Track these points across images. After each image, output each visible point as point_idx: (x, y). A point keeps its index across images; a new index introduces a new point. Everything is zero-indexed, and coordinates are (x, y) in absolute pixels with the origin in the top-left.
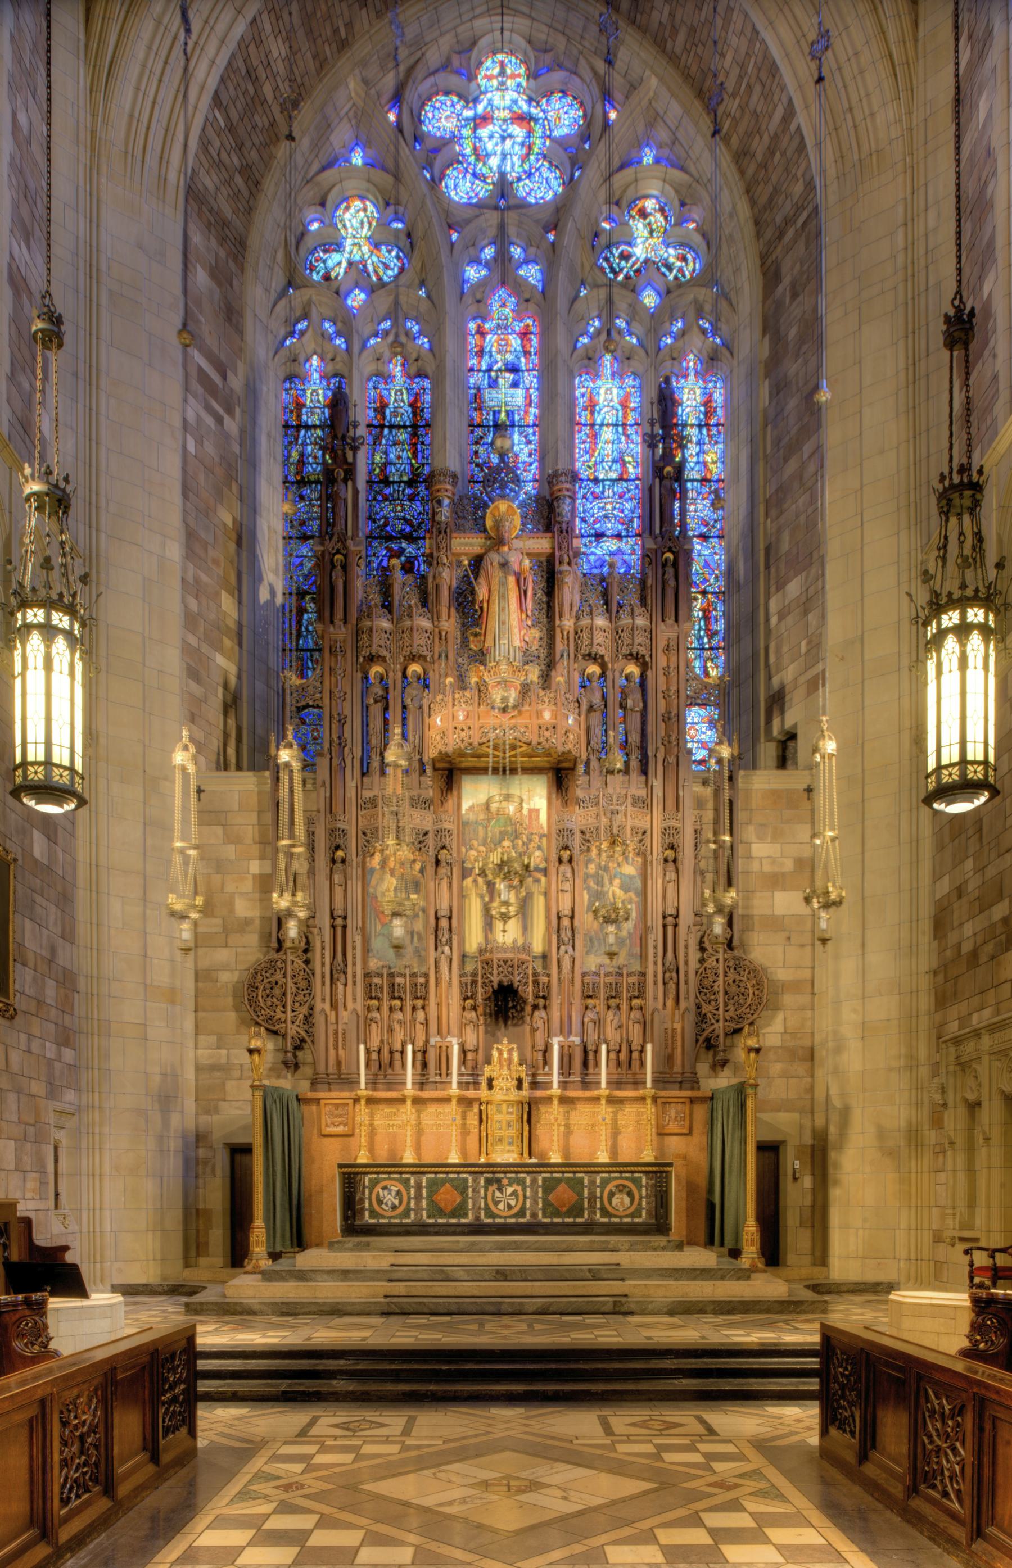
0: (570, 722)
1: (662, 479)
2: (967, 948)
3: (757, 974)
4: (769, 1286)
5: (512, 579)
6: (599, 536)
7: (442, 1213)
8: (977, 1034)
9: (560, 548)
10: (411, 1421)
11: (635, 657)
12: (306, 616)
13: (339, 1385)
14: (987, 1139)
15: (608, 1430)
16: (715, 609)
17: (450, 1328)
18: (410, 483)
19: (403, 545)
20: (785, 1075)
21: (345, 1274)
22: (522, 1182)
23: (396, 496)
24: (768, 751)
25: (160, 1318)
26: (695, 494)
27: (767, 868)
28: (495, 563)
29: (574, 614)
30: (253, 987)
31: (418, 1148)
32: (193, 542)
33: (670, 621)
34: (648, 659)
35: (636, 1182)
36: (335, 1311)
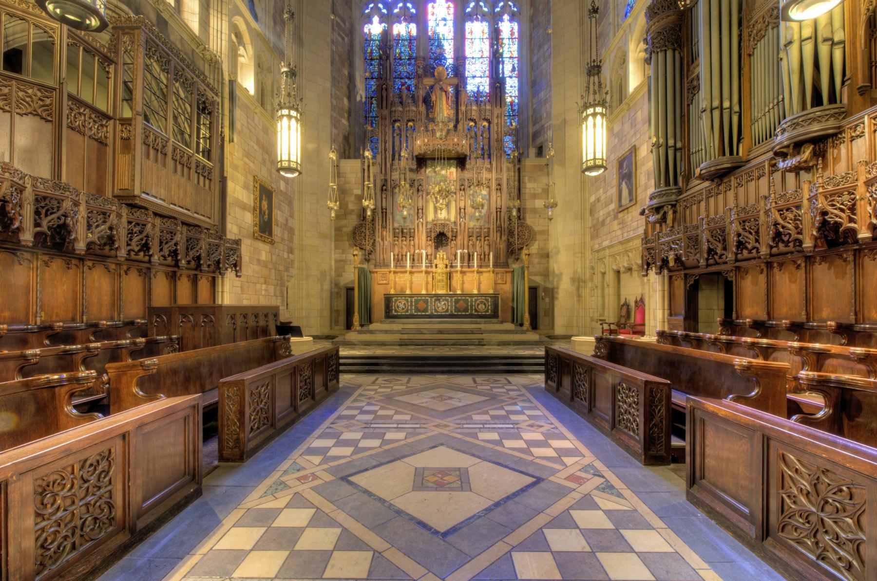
2: (601, 219)
3: (529, 228)
4: (533, 336)
6: (474, 77)
7: (420, 311)
8: (604, 249)
10: (410, 379)
11: (485, 119)
13: (384, 368)
14: (608, 285)
15: (475, 382)
17: (422, 350)
18: (409, 59)
20: (539, 263)
21: (386, 332)
22: (447, 300)
24: (532, 151)
25: (325, 346)
27: (532, 192)
30: (354, 233)
31: (411, 289)
32: (334, 81)
35: (487, 300)
36: (383, 344)
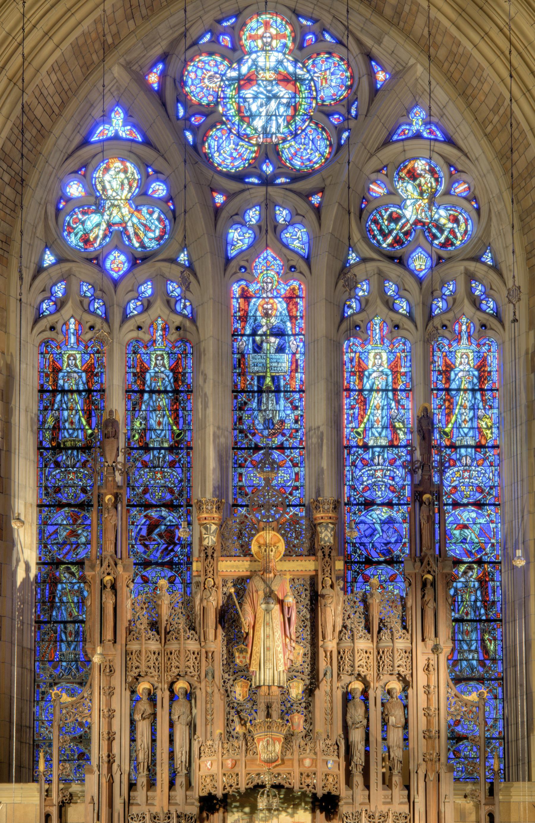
0: (329, 766)
5: (276, 608)
12: (59, 587)
26: (469, 461)
34: (408, 678)
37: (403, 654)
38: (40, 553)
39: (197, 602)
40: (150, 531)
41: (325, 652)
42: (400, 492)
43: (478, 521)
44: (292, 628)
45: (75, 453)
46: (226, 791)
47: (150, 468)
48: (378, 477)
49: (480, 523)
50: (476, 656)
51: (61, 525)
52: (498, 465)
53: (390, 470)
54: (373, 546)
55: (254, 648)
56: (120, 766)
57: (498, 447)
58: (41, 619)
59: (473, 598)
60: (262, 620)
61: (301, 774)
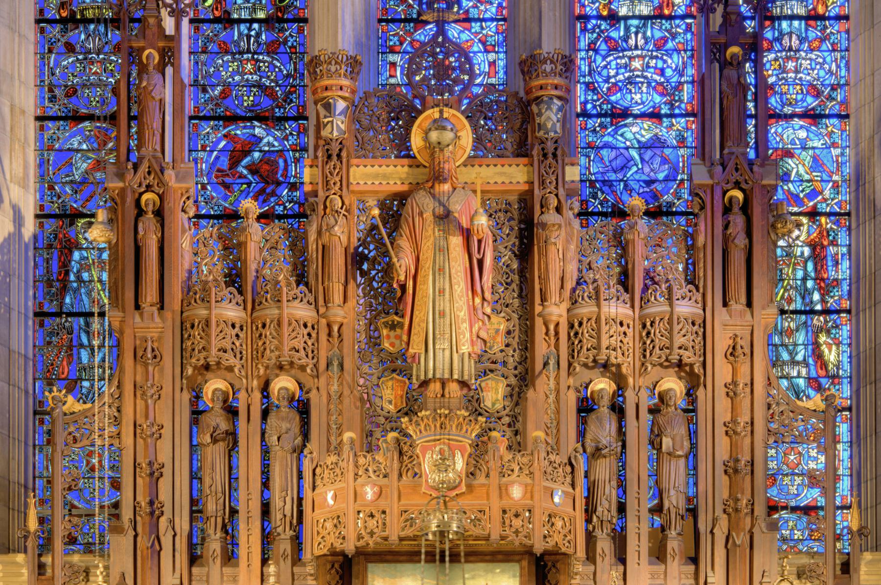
0: (557, 499)
1: (725, 64)
5: (456, 241)
9: (542, 183)
12: (76, 255)
16: (834, 243)
19: (258, 131)
23: (243, 45)
26: (795, 42)
28: (428, 215)
29: (567, 293)
33: (738, 306)
34: (697, 369)
37: (689, 327)
38: (42, 199)
39: (312, 237)
40: (234, 163)
41: (546, 324)
42: (674, 94)
43: (810, 144)
44: (485, 278)
45: (102, 28)
46: (361, 543)
47: (233, 54)
48: (636, 69)
49: (814, 148)
50: (804, 371)
51: (78, 151)
52: (847, 50)
53: (656, 57)
54: (626, 186)
55: (416, 313)
56: (172, 522)
57: (847, 18)
58: (46, 309)
59: (800, 274)
60: (430, 263)
61: (504, 512)
